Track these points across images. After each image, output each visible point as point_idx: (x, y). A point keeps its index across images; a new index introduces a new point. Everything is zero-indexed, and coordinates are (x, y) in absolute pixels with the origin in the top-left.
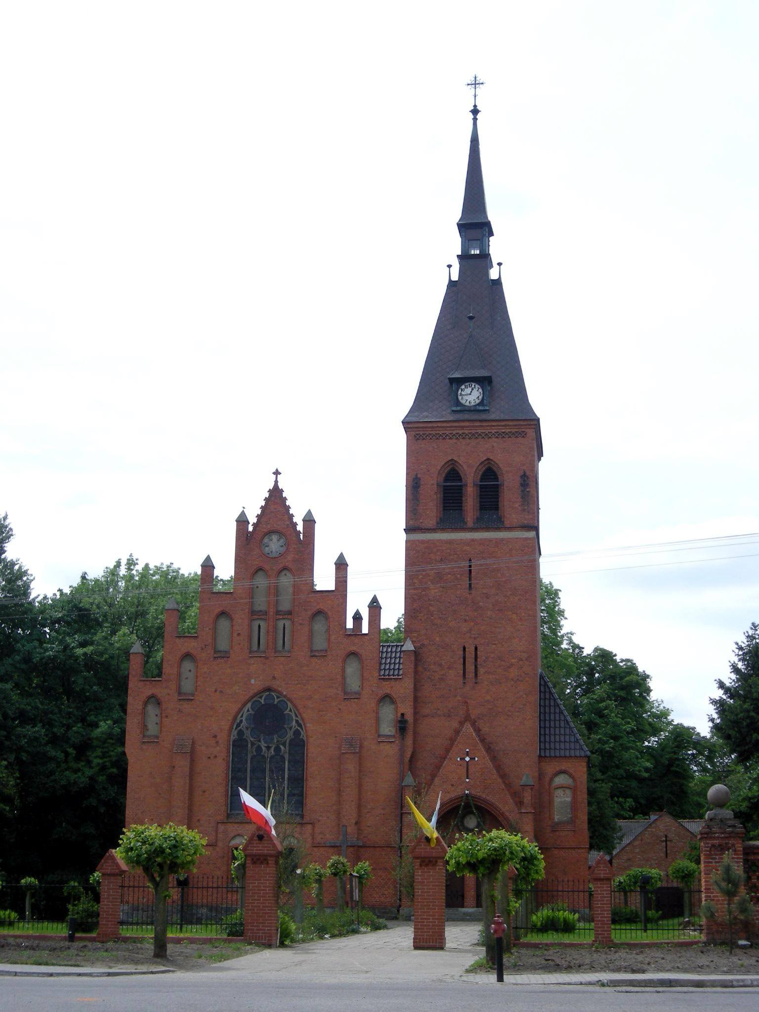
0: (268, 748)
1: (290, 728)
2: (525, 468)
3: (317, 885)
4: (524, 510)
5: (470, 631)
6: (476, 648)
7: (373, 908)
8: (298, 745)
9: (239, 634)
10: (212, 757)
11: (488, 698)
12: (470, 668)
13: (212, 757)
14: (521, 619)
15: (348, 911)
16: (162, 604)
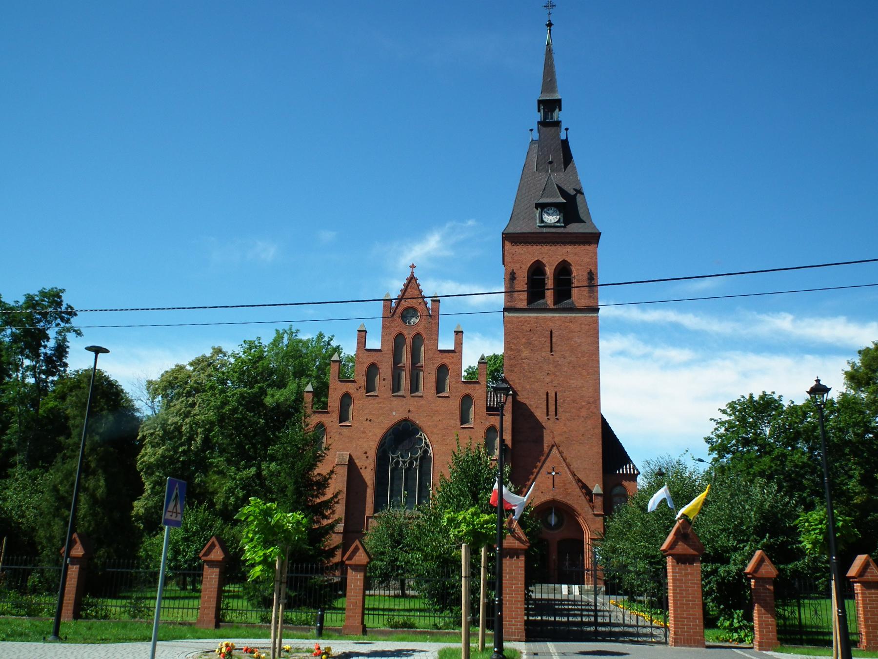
0: (404, 462)
1: (421, 448)
3: (274, 463)
5: (552, 381)
7: (665, 623)
8: (425, 459)
11: (565, 429)
12: (552, 408)
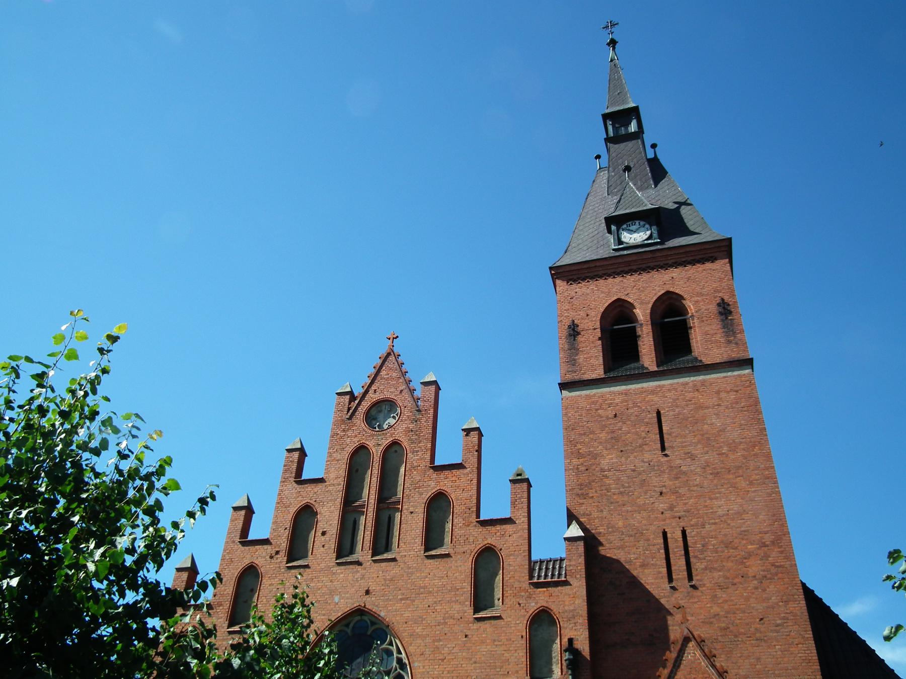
2: (720, 295)
4: (730, 342)
5: (671, 508)
6: (684, 532)
9: (324, 533)
10: (106, 345)
12: (679, 564)
13: (106, 345)
14: (751, 483)
15: (178, 631)
16: (262, 665)
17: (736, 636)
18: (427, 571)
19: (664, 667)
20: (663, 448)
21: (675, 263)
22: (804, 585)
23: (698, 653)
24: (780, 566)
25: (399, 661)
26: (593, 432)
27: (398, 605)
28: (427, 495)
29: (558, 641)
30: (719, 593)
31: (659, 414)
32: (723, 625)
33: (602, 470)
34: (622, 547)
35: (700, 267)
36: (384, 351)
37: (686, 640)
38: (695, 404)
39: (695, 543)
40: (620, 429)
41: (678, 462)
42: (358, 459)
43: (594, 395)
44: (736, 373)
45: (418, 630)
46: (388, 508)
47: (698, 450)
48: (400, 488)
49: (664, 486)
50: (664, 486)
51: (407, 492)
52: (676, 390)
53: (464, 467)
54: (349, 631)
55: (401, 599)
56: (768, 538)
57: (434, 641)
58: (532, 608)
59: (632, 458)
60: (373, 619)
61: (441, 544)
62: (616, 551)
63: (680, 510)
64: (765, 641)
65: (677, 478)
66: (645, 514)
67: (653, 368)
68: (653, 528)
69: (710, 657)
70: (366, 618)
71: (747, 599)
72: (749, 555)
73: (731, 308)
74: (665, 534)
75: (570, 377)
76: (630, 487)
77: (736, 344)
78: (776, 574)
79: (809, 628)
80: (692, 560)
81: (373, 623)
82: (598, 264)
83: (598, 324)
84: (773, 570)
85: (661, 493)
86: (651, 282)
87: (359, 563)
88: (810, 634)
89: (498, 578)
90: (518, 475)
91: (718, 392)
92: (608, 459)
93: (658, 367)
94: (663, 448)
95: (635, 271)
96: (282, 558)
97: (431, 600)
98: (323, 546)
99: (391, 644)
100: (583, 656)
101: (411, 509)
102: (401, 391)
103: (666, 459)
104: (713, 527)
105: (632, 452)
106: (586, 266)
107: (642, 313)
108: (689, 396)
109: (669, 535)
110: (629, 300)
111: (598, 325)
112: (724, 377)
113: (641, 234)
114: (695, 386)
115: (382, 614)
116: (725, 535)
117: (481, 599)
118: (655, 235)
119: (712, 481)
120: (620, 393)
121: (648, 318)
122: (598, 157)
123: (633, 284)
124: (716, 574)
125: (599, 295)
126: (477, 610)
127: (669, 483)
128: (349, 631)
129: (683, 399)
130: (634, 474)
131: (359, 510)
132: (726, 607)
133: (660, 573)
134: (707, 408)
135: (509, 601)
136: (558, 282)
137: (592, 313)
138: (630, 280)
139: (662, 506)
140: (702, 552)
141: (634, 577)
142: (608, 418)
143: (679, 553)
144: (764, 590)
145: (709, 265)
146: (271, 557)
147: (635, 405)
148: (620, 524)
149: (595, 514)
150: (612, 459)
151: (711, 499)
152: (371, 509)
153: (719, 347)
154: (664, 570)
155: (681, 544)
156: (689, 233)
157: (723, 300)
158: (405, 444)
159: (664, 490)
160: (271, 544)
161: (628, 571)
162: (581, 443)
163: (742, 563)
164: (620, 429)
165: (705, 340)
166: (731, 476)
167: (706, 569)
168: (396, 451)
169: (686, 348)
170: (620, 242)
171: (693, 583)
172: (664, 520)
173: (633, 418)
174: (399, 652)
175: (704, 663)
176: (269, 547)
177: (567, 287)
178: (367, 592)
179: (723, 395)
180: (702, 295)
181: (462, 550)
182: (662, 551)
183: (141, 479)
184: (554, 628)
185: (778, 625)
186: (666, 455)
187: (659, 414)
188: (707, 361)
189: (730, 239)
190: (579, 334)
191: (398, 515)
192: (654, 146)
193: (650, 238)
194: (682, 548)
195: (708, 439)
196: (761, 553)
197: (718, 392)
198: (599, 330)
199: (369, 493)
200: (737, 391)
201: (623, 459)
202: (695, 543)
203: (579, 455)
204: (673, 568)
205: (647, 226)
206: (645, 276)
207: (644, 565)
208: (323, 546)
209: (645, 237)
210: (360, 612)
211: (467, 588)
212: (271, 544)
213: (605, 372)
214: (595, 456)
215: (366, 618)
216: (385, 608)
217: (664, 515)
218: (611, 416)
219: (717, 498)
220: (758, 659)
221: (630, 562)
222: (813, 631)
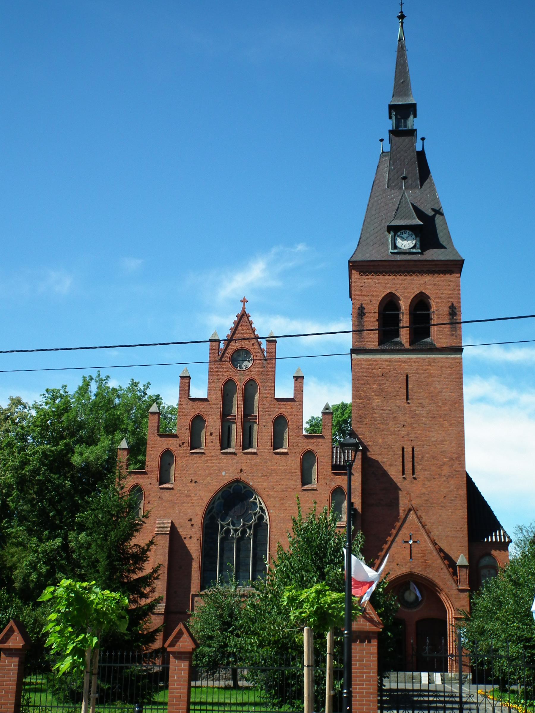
2: (452, 300)
4: (452, 335)
5: (408, 435)
6: (413, 449)
9: (211, 434)
17: (432, 504)
18: (275, 461)
19: (398, 522)
20: (407, 399)
21: (429, 271)
22: (467, 474)
23: (415, 516)
24: (458, 471)
25: (261, 508)
26: (368, 384)
27: (259, 480)
28: (273, 416)
29: (316, 464)
30: (426, 482)
31: (407, 376)
32: (426, 498)
33: (373, 408)
34: (380, 454)
35: (442, 277)
36: (239, 311)
37: (410, 510)
38: (428, 373)
39: (418, 455)
40: (385, 384)
41: (415, 408)
42: (228, 390)
43: (371, 360)
44: (453, 356)
45: (272, 493)
46: (249, 421)
47: (425, 402)
48: (256, 409)
49: (406, 422)
50: (406, 422)
51: (261, 413)
52: (418, 362)
53: (295, 401)
54: (231, 491)
55: (262, 476)
56: (454, 456)
57: (281, 500)
58: (334, 485)
59: (390, 403)
60: (245, 485)
61: (281, 446)
62: (377, 456)
63: (412, 436)
64: (445, 508)
65: (413, 418)
66: (394, 437)
67: (407, 346)
68: (397, 445)
69: (419, 518)
70: (240, 484)
71: (440, 486)
72: (444, 464)
73: (456, 311)
74: (403, 449)
75: (358, 345)
76: (387, 420)
77: (456, 337)
78: (455, 475)
79: (466, 502)
80: (415, 464)
81: (245, 488)
82: (380, 263)
83: (377, 309)
84: (454, 473)
85: (404, 425)
86: (412, 283)
87: (235, 454)
88: (466, 506)
89: (343, 505)
90: (327, 409)
91: (441, 368)
92: (377, 401)
93: (410, 345)
94: (407, 399)
95: (403, 272)
96: (187, 446)
97: (278, 478)
98: (212, 442)
99: (255, 499)
100: (358, 512)
101: (264, 424)
102: (253, 344)
103: (408, 405)
104: (428, 447)
105: (391, 399)
106: (372, 264)
107: (404, 305)
108: (425, 367)
109: (405, 450)
110: (398, 294)
111: (377, 310)
112: (447, 358)
113: (410, 242)
114: (429, 361)
115: (251, 484)
116: (434, 452)
117: (305, 480)
118: (418, 246)
119: (431, 421)
120: (386, 360)
121: (408, 310)
122: (382, 140)
123: (400, 282)
124: (426, 473)
125: (380, 286)
126: (303, 484)
127: (408, 420)
128: (231, 491)
129: (422, 369)
130: (391, 412)
131: (232, 421)
132: (429, 489)
133: (398, 470)
134: (434, 376)
135: (322, 482)
136: (354, 272)
137: (374, 301)
138: (399, 279)
139: (403, 433)
140: (421, 460)
141: (385, 471)
142: (379, 376)
143: (410, 460)
144: (448, 483)
145: (448, 277)
146: (180, 446)
147: (394, 369)
148: (380, 441)
149: (367, 434)
150: (378, 402)
151: (429, 432)
152: (239, 422)
153: (446, 337)
154: (401, 468)
155: (411, 455)
156: (440, 246)
157: (453, 304)
158: (258, 382)
159: (405, 424)
160: (178, 438)
161: (382, 467)
162: (362, 390)
163: (440, 468)
164: (385, 384)
165: (438, 335)
166: (441, 420)
167: (421, 469)
168: (252, 385)
169: (427, 334)
170: (395, 247)
171: (415, 476)
172: (404, 441)
173: (392, 378)
174: (260, 504)
175: (416, 521)
176: (178, 440)
177: (359, 277)
178: (241, 471)
179: (444, 369)
180: (440, 298)
181: (295, 451)
182: (401, 458)
183: (333, 564)
184: (344, 496)
185: (452, 500)
186: (409, 403)
187: (407, 376)
188: (438, 345)
189: (464, 260)
190: (365, 314)
191: (255, 427)
192: (423, 139)
193: (414, 247)
194: (411, 457)
195: (432, 396)
196: (450, 463)
197: (441, 368)
198: (377, 314)
199: (237, 409)
200: (452, 368)
201: (385, 403)
202: (418, 455)
203: (360, 398)
204: (405, 468)
205: (414, 236)
206: (409, 278)
207: (390, 465)
208: (212, 442)
209: (412, 246)
210: (237, 481)
211: (298, 472)
212: (178, 438)
213: (379, 344)
214: (369, 399)
215: (240, 484)
216: (253, 481)
217: (403, 439)
218: (380, 374)
219: (432, 432)
220: (440, 516)
221: (384, 462)
222: (467, 504)
